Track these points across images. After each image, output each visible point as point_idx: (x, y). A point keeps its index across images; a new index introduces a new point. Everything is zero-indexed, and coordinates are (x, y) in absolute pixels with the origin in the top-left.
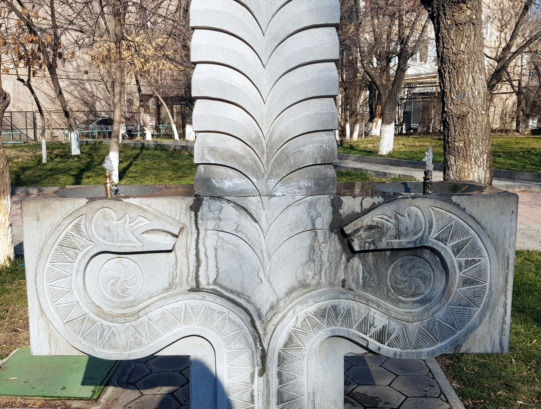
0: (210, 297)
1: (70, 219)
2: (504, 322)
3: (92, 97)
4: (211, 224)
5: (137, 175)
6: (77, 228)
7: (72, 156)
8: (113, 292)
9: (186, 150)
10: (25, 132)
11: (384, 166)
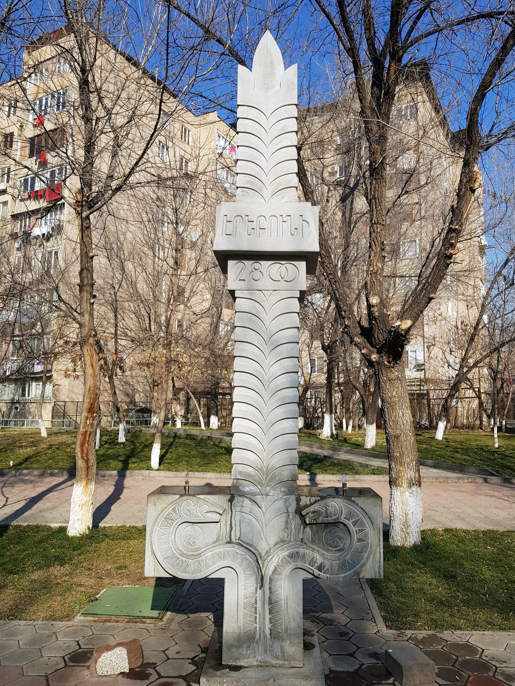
0: (236, 546)
1: (171, 505)
2: (380, 562)
3: (133, 390)
4: (238, 509)
5: (172, 461)
6: (174, 509)
7: (118, 443)
8: (189, 543)
9: (211, 440)
10: (74, 419)
11: (367, 458)
